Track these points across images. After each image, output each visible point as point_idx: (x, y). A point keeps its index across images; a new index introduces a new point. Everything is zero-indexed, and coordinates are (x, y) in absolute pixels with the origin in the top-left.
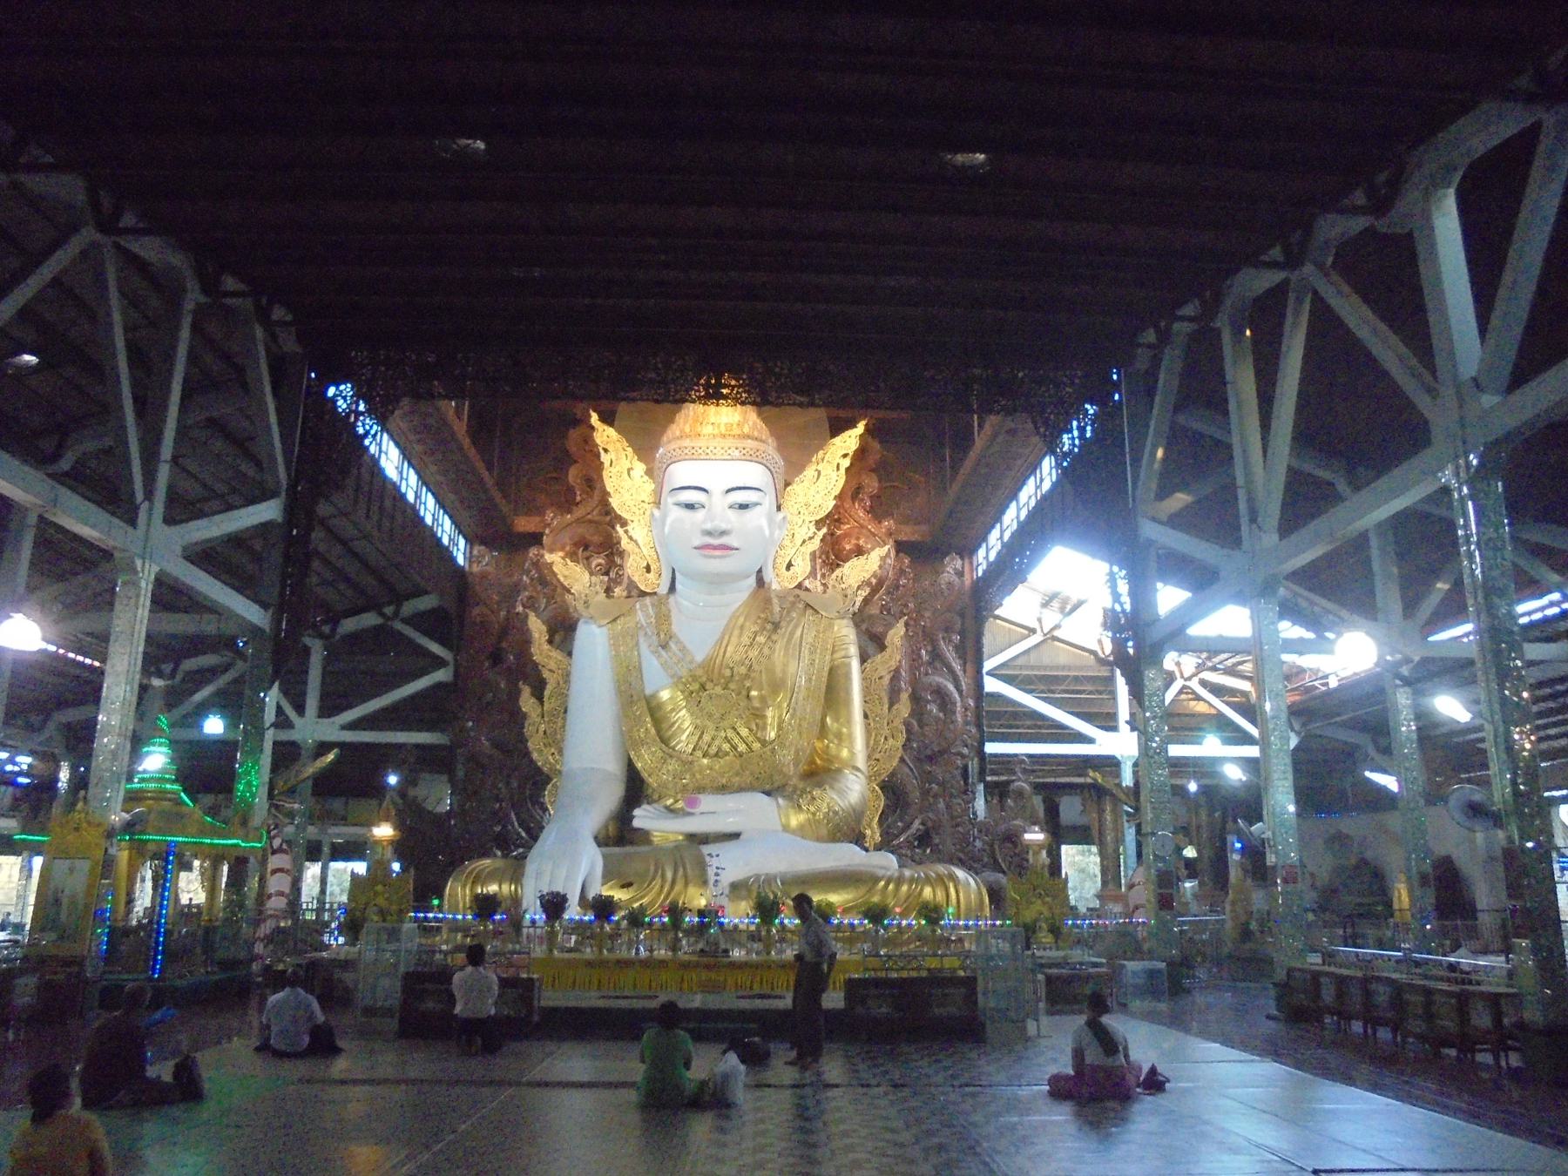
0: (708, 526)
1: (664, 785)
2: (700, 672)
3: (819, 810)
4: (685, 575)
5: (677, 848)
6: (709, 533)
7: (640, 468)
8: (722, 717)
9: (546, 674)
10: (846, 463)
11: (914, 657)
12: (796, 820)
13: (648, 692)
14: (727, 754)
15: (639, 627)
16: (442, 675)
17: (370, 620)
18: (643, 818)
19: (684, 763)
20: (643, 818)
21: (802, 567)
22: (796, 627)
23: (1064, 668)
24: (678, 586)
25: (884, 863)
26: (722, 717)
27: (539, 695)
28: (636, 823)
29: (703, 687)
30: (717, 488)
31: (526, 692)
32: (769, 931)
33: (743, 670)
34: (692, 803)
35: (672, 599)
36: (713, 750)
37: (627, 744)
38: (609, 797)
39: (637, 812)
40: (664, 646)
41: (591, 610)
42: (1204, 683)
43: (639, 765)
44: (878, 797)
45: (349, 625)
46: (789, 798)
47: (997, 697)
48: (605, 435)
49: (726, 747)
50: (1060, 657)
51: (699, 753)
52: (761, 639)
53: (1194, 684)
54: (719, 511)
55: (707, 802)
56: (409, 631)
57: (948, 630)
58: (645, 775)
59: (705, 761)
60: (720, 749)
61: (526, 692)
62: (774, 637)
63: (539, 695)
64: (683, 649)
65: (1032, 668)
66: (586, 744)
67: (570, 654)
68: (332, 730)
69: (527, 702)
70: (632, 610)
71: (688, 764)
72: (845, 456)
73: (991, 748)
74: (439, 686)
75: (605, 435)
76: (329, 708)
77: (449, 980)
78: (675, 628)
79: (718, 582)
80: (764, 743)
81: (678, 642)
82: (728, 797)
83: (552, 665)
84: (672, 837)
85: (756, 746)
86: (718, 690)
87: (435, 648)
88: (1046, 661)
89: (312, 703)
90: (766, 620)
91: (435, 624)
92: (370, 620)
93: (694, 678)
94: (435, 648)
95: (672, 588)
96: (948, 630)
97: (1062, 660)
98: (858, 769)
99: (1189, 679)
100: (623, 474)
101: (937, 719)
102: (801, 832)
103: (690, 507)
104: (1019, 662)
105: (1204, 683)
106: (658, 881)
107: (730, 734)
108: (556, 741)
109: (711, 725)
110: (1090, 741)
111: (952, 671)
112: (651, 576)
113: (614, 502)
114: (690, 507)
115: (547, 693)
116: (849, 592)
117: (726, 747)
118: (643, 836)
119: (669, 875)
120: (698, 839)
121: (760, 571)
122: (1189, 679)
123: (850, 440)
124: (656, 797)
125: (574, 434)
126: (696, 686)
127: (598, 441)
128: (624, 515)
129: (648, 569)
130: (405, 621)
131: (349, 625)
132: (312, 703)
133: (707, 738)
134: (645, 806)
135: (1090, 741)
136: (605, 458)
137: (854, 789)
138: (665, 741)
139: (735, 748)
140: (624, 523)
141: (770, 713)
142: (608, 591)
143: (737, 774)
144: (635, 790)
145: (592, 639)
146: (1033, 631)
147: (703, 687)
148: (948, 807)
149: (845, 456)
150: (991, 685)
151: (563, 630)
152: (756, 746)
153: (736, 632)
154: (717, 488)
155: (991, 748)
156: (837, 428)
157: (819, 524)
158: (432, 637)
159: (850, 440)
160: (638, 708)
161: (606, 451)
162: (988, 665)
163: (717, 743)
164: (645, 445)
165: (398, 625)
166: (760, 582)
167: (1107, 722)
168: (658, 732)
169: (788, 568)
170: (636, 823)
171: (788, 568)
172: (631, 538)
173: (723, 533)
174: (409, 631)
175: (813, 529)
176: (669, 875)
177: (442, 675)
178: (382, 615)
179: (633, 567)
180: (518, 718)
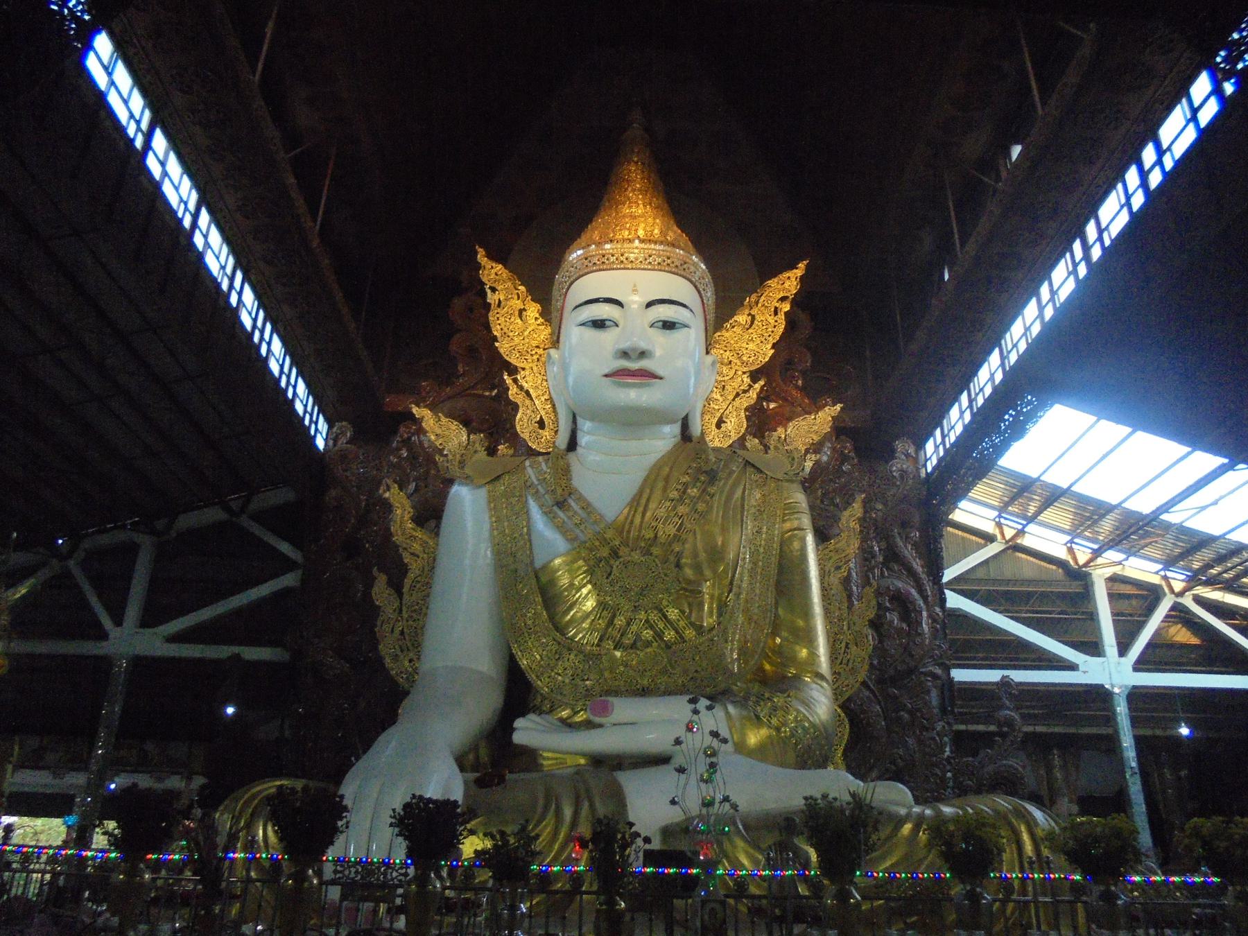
0: (624, 345)
1: (559, 689)
2: (609, 534)
3: (785, 724)
4: (594, 416)
5: (579, 771)
6: (625, 354)
7: (533, 310)
8: (642, 593)
9: (407, 559)
10: (786, 307)
11: (866, 556)
12: (754, 738)
13: (538, 564)
14: (648, 644)
15: (528, 486)
16: (289, 580)
17: (213, 515)
18: (526, 731)
19: (588, 657)
20: (526, 731)
21: (736, 424)
22: (735, 486)
23: (1030, 582)
24: (583, 440)
25: (893, 796)
26: (642, 593)
27: (396, 586)
28: (518, 738)
29: (615, 554)
30: (635, 301)
31: (382, 579)
32: (843, 896)
33: (671, 530)
34: (605, 709)
35: (572, 457)
36: (627, 641)
37: (509, 633)
38: (480, 707)
39: (519, 723)
40: (561, 504)
41: (467, 470)
42: (1199, 600)
43: (524, 663)
44: (841, 723)
45: (187, 521)
46: (742, 703)
47: (959, 617)
48: (492, 272)
49: (647, 634)
50: (1028, 568)
51: (609, 644)
52: (693, 492)
53: (1188, 601)
54: (635, 327)
55: (623, 709)
56: (257, 530)
57: (904, 525)
58: (532, 677)
59: (618, 654)
60: (638, 636)
61: (382, 579)
62: (711, 490)
63: (396, 586)
64: (587, 506)
65: (995, 581)
66: (459, 632)
67: (437, 534)
68: (154, 643)
69: (381, 592)
70: (520, 468)
71: (591, 658)
72: (783, 299)
73: (960, 675)
74: (285, 593)
75: (492, 272)
76: (150, 619)
77: (1118, 812)
78: (576, 482)
79: (634, 421)
80: (699, 629)
81: (581, 498)
82: (652, 701)
83: (416, 547)
84: (570, 761)
85: (690, 633)
86: (636, 556)
87: (285, 547)
88: (1008, 574)
89: (133, 612)
90: (699, 470)
91: (285, 521)
92: (213, 515)
93: (605, 542)
94: (285, 547)
95: (572, 445)
96: (904, 525)
97: (1028, 573)
98: (822, 677)
99: (1181, 594)
100: (515, 322)
101: (899, 631)
102: (760, 753)
103: (599, 324)
104: (980, 574)
105: (1199, 600)
106: (550, 819)
107: (654, 616)
108: (413, 642)
109: (626, 606)
110: (1072, 667)
111: (911, 573)
112: (546, 433)
113: (503, 347)
114: (599, 324)
115: (405, 590)
116: (796, 455)
117: (647, 634)
118: (528, 758)
119: (568, 812)
120: (607, 764)
121: (687, 416)
122: (1181, 594)
123: (789, 282)
124: (547, 707)
125: (458, 303)
126: (605, 552)
127: (485, 280)
128: (513, 361)
129: (541, 424)
130: (256, 517)
131: (187, 521)
132: (133, 612)
133: (620, 621)
134: (532, 716)
135: (1072, 667)
136: (491, 298)
137: (820, 704)
138: (560, 629)
139: (659, 635)
140: (513, 370)
141: (706, 587)
142: (492, 451)
143: (664, 671)
144: (518, 694)
145: (468, 504)
146: (990, 539)
147: (615, 554)
148: (920, 742)
149: (783, 299)
150: (954, 600)
151: (430, 514)
152: (690, 633)
153: (660, 484)
154: (635, 301)
155: (960, 675)
156: (769, 269)
157: (755, 376)
158: (285, 538)
159: (789, 282)
160: (525, 589)
161: (493, 290)
162: (949, 574)
163: (634, 628)
164: (543, 287)
165: (245, 521)
166: (686, 435)
167: (1093, 648)
168: (551, 618)
169: (718, 426)
170: (518, 738)
171: (718, 426)
172: (521, 388)
173: (643, 354)
174: (257, 530)
175: (747, 380)
176: (568, 812)
177: (289, 580)
178: (228, 509)
179: (523, 423)
180: (371, 612)
